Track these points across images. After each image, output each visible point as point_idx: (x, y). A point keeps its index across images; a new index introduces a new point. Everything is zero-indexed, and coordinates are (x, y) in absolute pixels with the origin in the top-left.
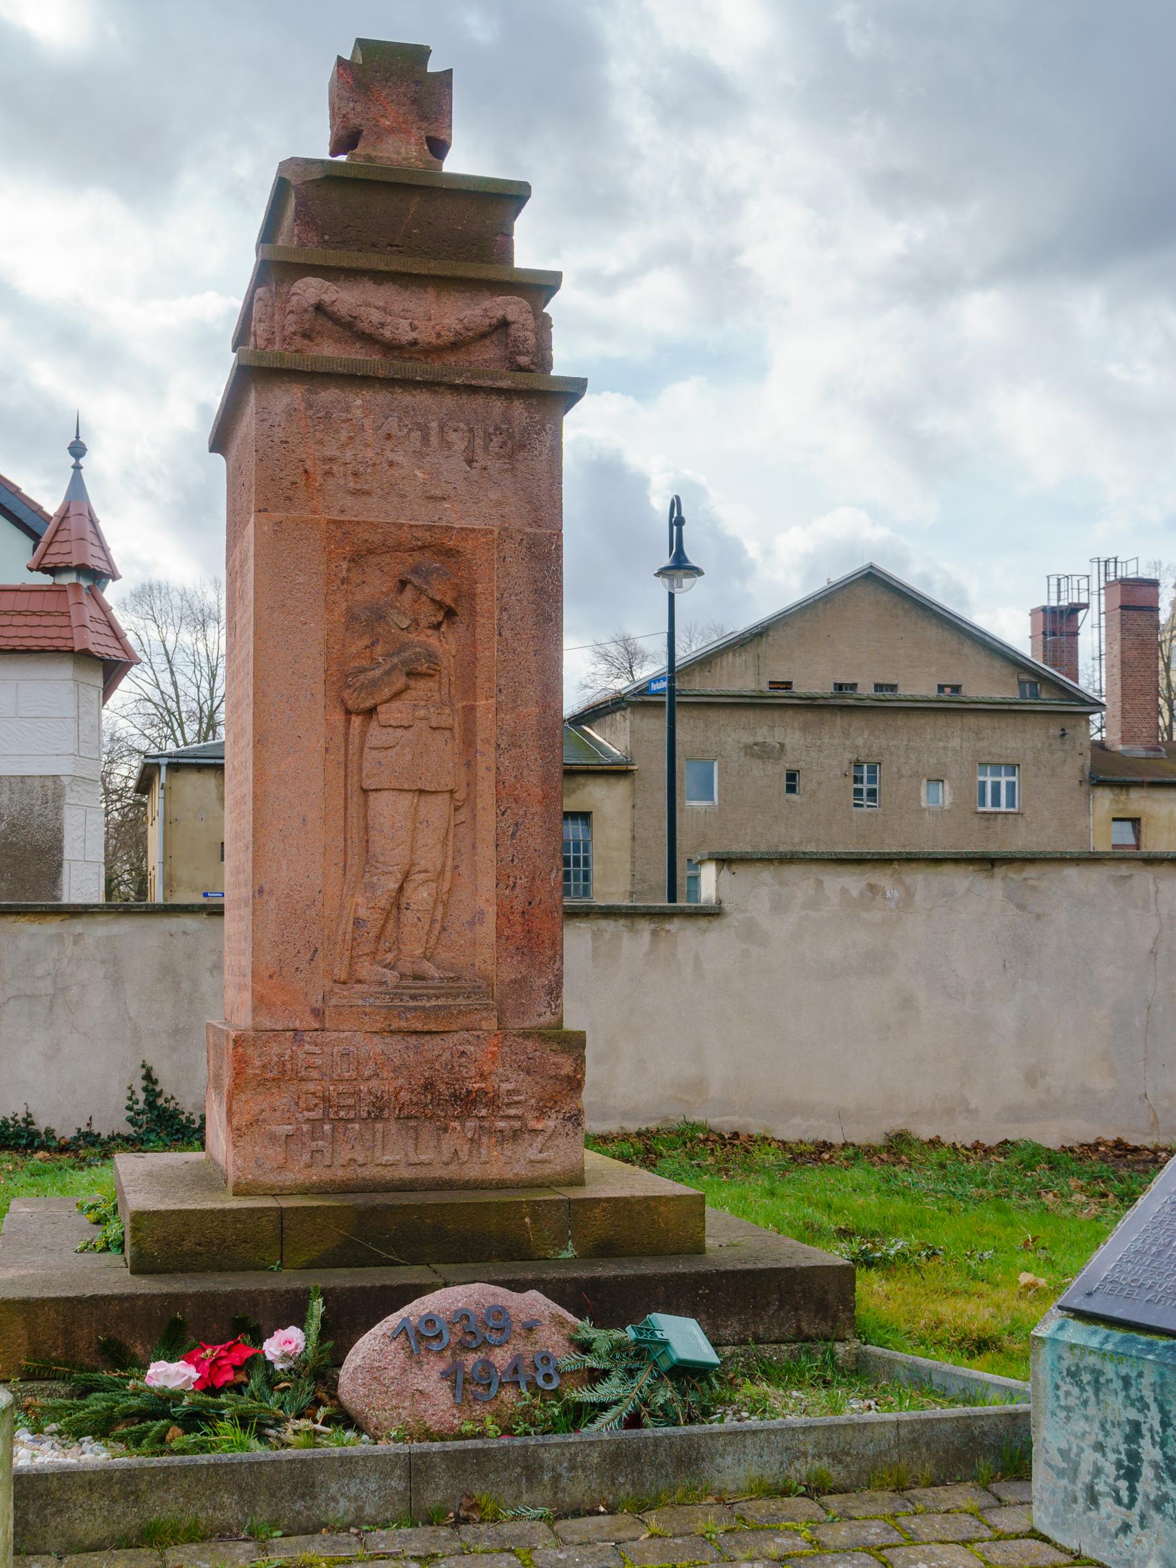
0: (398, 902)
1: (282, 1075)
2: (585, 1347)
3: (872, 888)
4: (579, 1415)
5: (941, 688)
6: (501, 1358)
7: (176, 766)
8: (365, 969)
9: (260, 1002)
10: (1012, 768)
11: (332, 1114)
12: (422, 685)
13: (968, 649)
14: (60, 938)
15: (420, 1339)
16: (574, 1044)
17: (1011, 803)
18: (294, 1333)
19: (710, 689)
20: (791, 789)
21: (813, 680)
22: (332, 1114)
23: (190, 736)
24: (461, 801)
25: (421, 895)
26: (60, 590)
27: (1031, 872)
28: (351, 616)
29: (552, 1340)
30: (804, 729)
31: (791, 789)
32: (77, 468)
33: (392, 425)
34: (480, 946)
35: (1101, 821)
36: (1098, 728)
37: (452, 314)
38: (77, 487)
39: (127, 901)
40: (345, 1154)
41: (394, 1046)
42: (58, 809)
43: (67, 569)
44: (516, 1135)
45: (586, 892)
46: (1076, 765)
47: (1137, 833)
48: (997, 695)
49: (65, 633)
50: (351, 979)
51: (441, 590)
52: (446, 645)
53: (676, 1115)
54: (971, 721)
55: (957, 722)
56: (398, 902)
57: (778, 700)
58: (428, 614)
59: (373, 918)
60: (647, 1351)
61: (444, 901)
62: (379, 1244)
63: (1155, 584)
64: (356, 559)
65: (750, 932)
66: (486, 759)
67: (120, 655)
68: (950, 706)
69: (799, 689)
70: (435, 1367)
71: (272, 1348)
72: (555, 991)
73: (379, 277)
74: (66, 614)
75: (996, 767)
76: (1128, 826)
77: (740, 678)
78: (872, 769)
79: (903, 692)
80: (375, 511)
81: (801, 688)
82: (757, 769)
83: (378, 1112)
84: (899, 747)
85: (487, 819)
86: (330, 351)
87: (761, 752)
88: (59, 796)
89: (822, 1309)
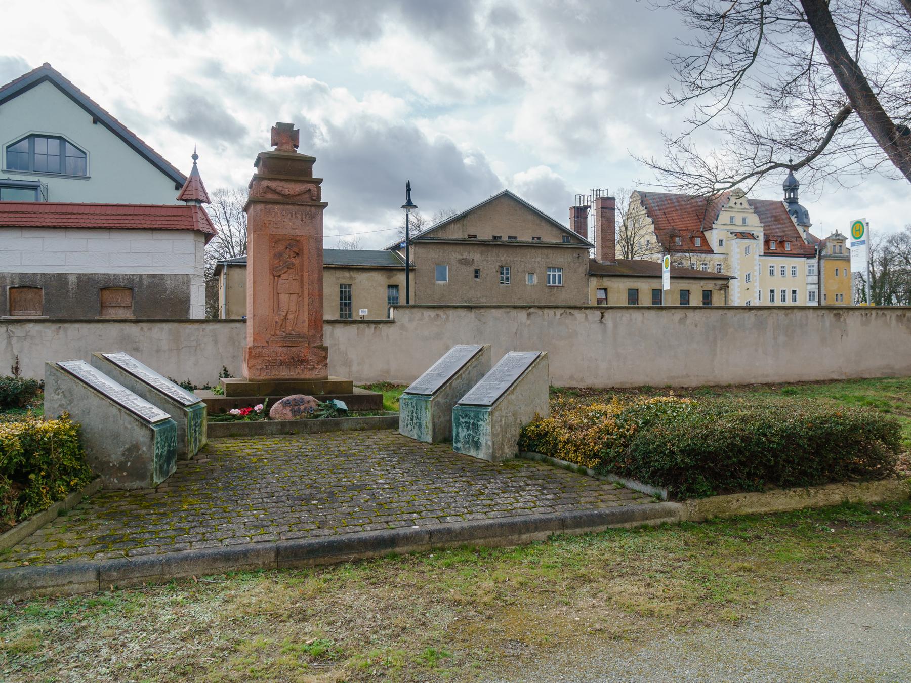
0: (286, 317)
1: (259, 356)
2: (319, 405)
3: (437, 315)
4: (318, 416)
5: (533, 238)
6: (302, 407)
7: (230, 266)
8: (278, 332)
9: (254, 340)
10: (560, 269)
11: (271, 364)
12: (291, 271)
13: (543, 224)
14: (198, 329)
15: (286, 404)
16: (325, 349)
17: (560, 283)
18: (261, 406)
19: (445, 237)
20: (476, 277)
21: (485, 233)
22: (271, 364)
23: (236, 252)
24: (300, 296)
25: (291, 316)
26: (189, 208)
27: (482, 310)
28: (275, 255)
29: (313, 404)
30: (481, 253)
31: (476, 277)
32: (195, 163)
33: (284, 213)
34: (304, 327)
35: (593, 290)
36: (592, 254)
37: (297, 188)
38: (195, 169)
39: (214, 317)
40: (274, 373)
41: (285, 349)
42: (189, 286)
43: (191, 200)
44: (312, 369)
45: (350, 316)
46: (583, 269)
47: (606, 294)
48: (554, 241)
49: (191, 223)
50: (275, 335)
51: (295, 249)
52: (296, 261)
53: (381, 380)
54: (545, 251)
55: (539, 251)
56: (286, 317)
57: (472, 242)
58: (292, 254)
59: (280, 322)
60: (333, 406)
61: (296, 318)
62: (279, 389)
63: (614, 199)
64: (276, 242)
65: (403, 327)
66: (306, 287)
67: (211, 231)
68: (537, 245)
69: (480, 238)
70: (289, 409)
71: (256, 408)
72: (322, 337)
73: (281, 180)
74: (191, 216)
75: (554, 269)
76: (603, 291)
77: (457, 233)
78: (507, 269)
79: (519, 239)
80: (281, 232)
81: (480, 237)
82: (463, 269)
83: (281, 363)
84: (519, 261)
85: (306, 300)
86: (270, 196)
87: (465, 262)
88: (189, 282)
89: (376, 403)
